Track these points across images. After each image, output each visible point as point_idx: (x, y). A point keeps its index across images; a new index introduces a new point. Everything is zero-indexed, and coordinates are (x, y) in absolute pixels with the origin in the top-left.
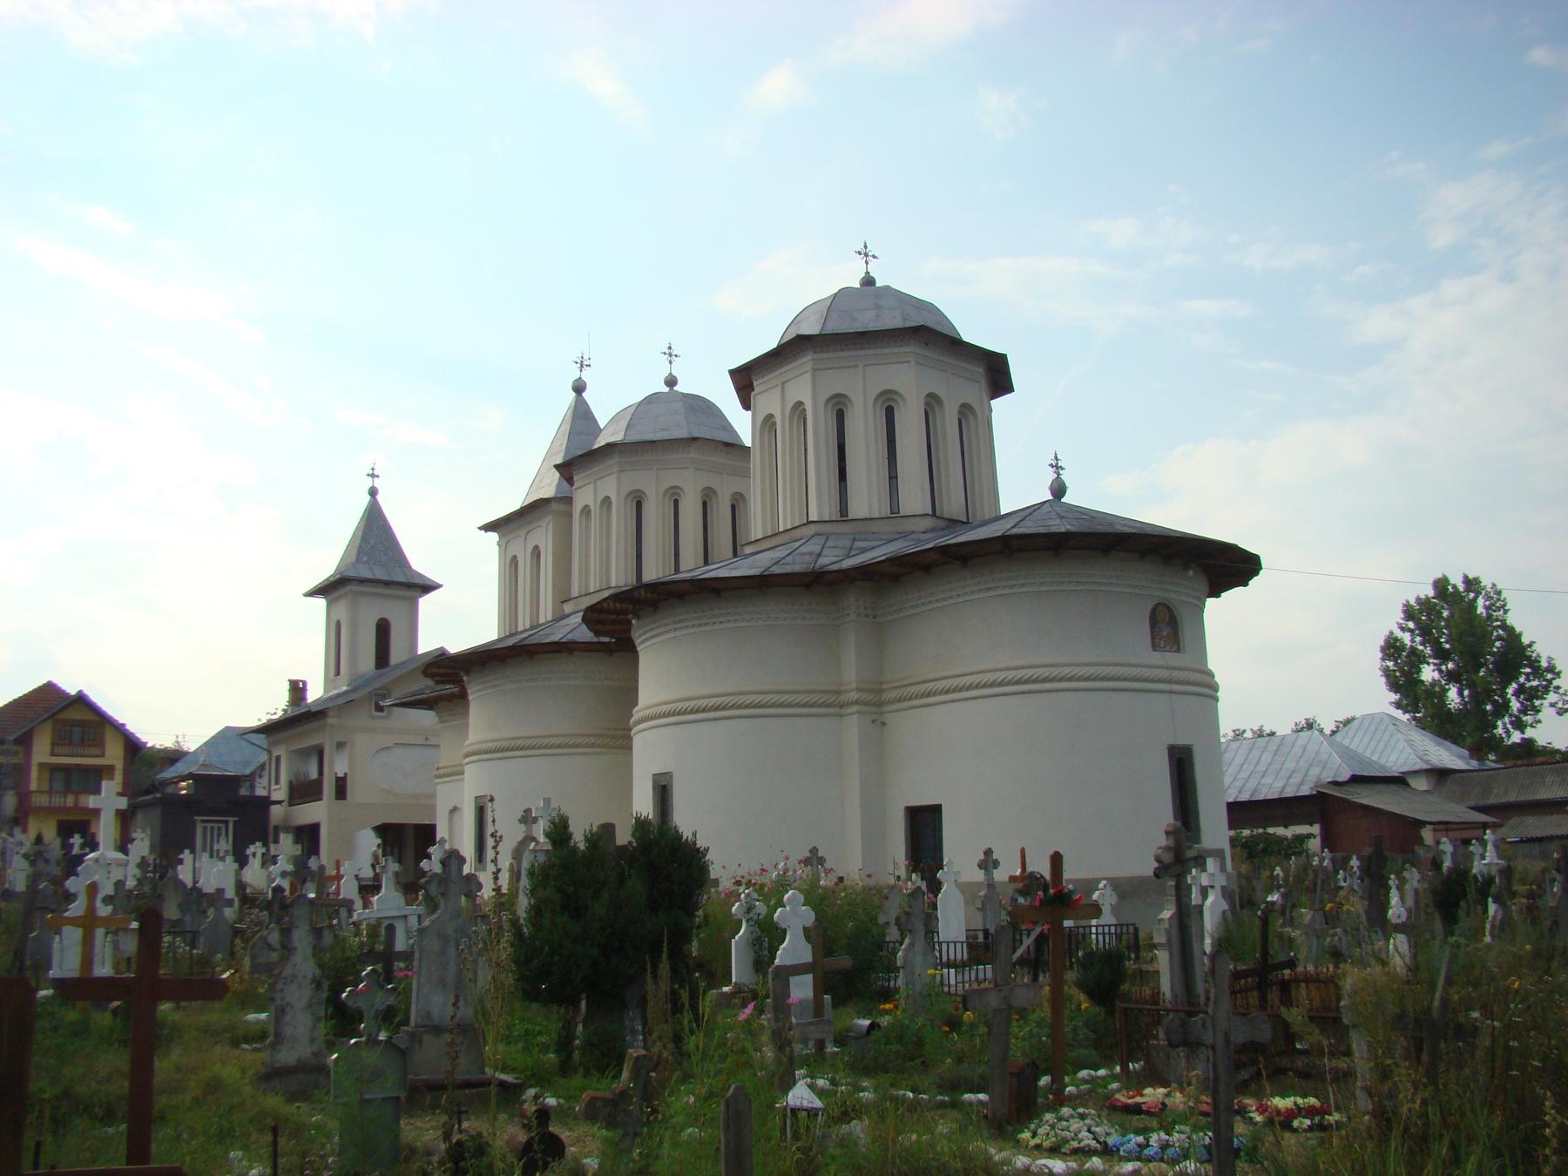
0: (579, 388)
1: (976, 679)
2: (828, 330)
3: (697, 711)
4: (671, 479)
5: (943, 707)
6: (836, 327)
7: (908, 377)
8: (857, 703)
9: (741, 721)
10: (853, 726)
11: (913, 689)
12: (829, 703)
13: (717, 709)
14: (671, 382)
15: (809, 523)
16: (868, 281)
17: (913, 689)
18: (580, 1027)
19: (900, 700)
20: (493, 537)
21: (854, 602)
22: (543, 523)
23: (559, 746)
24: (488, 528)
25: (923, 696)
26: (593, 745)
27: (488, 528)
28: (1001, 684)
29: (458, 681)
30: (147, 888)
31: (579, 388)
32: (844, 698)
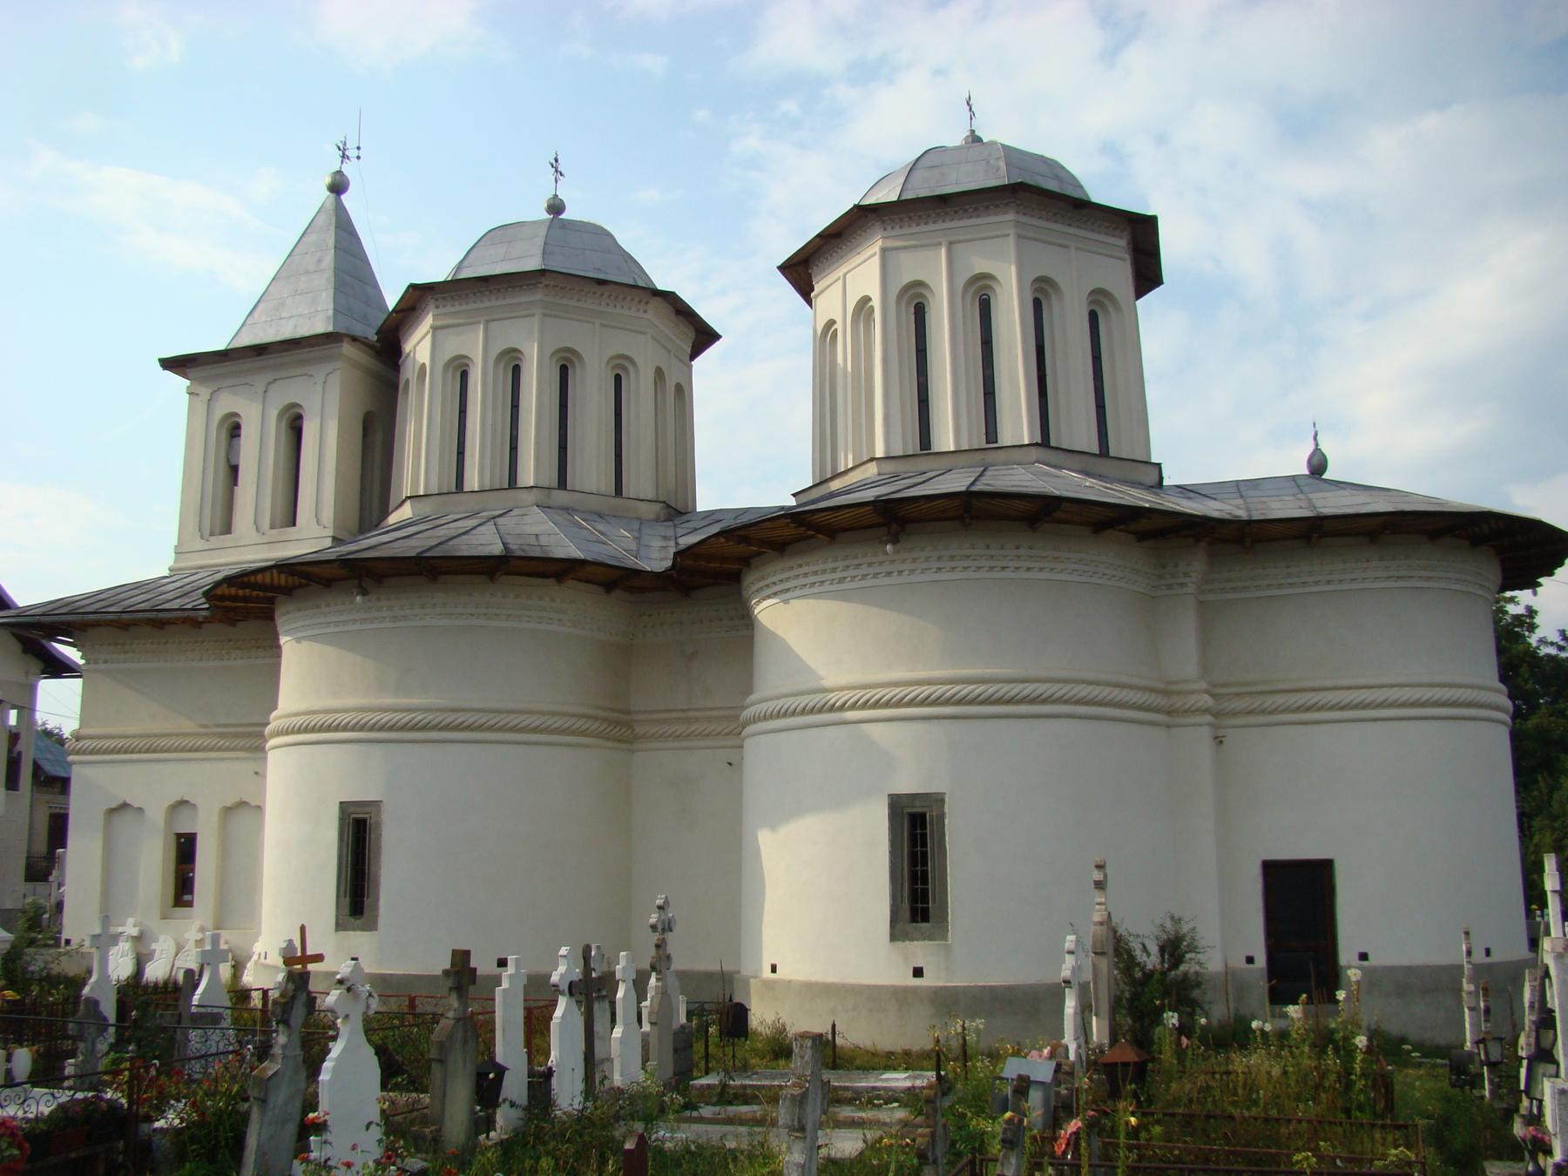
0: (338, 187)
1: (1394, 694)
2: (908, 196)
3: (887, 705)
4: (621, 343)
5: (796, 734)
6: (923, 188)
7: (598, 341)
8: (1207, 711)
9: (896, 726)
10: (1198, 738)
11: (1280, 700)
12: (1163, 708)
13: (1033, 701)
14: (556, 207)
15: (872, 459)
16: (975, 139)
17: (1280, 700)
18: (157, 1125)
19: (1251, 712)
20: (178, 384)
21: (1195, 565)
22: (319, 372)
23: (536, 730)
24: (174, 364)
25: (1298, 710)
26: (584, 733)
27: (174, 364)
28: (1424, 705)
29: (272, 601)
30: (1009, 1134)
31: (338, 187)
32: (1178, 702)
